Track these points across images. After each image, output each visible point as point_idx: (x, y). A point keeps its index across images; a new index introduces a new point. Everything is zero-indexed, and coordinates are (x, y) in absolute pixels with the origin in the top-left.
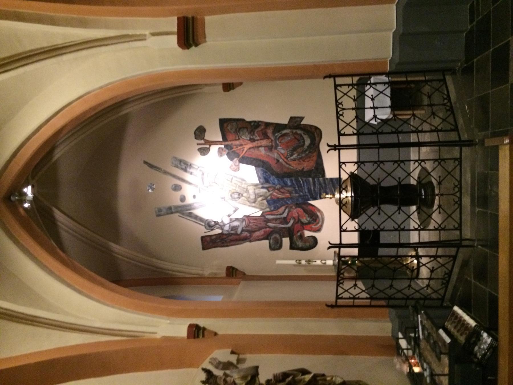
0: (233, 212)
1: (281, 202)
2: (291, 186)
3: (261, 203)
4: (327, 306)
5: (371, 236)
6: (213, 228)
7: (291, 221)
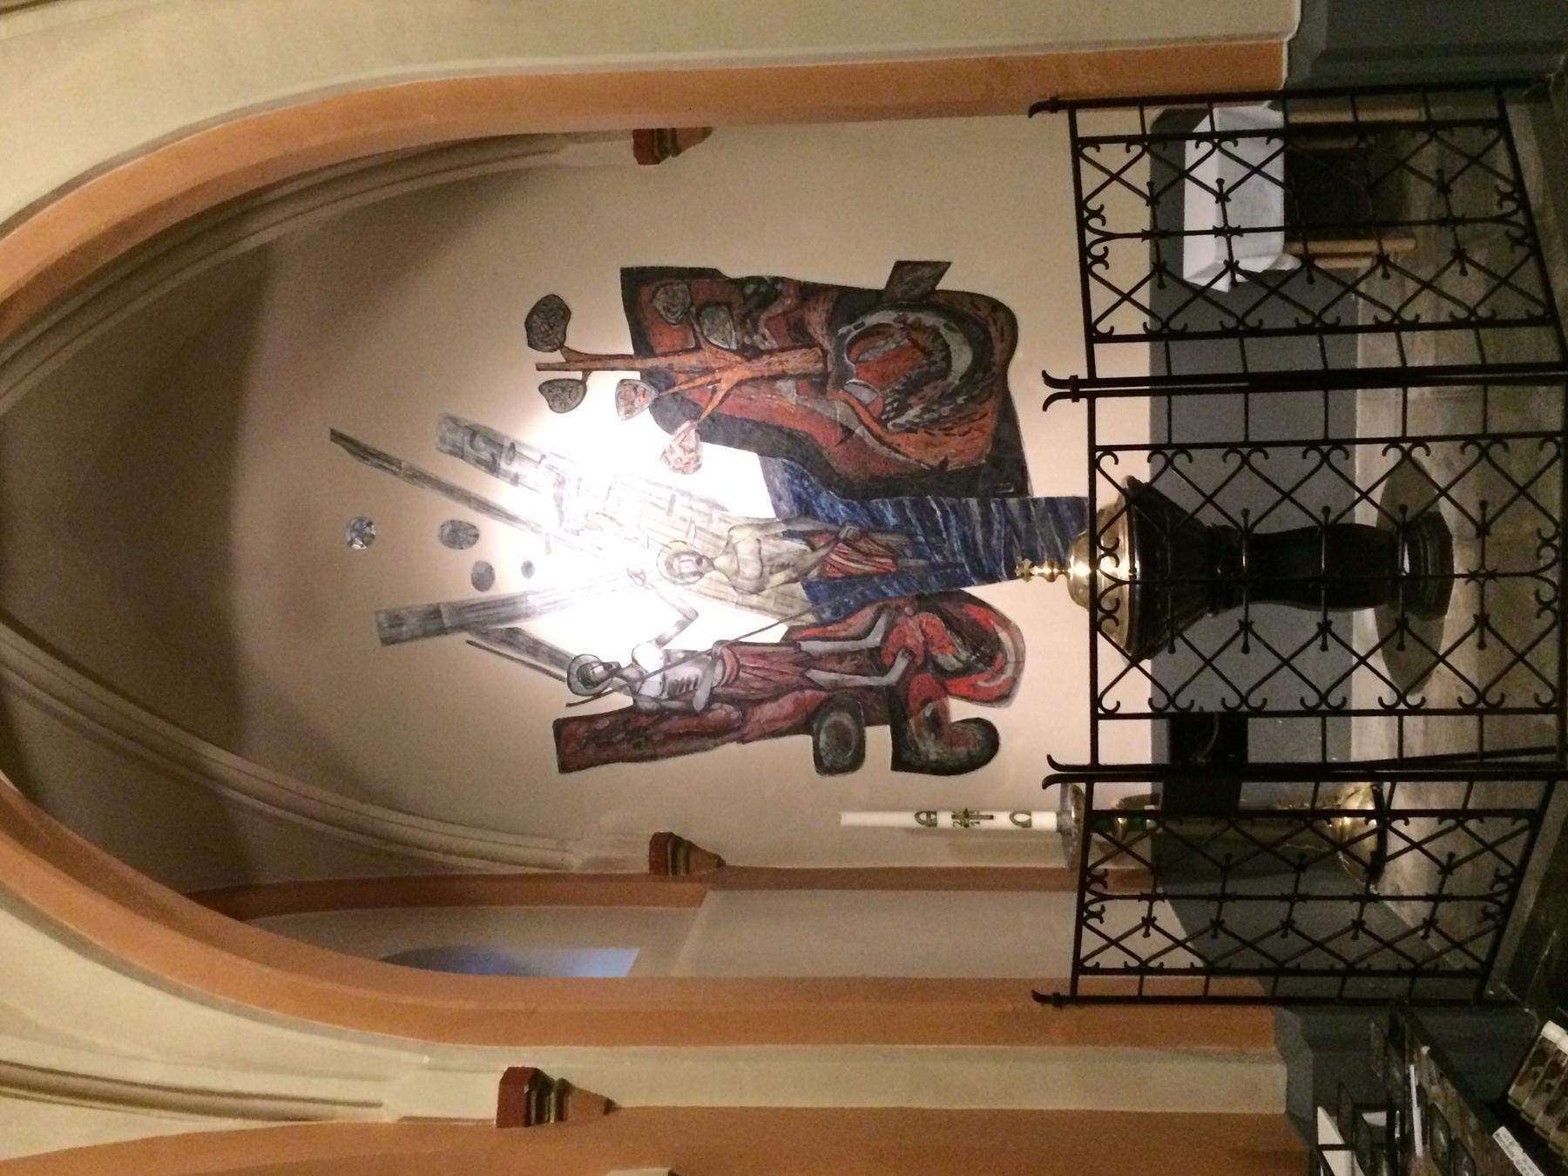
0: (675, 629)
1: (861, 588)
2: (896, 530)
3: (784, 594)
4: (1040, 998)
5: (1216, 733)
6: (599, 688)
7: (896, 663)
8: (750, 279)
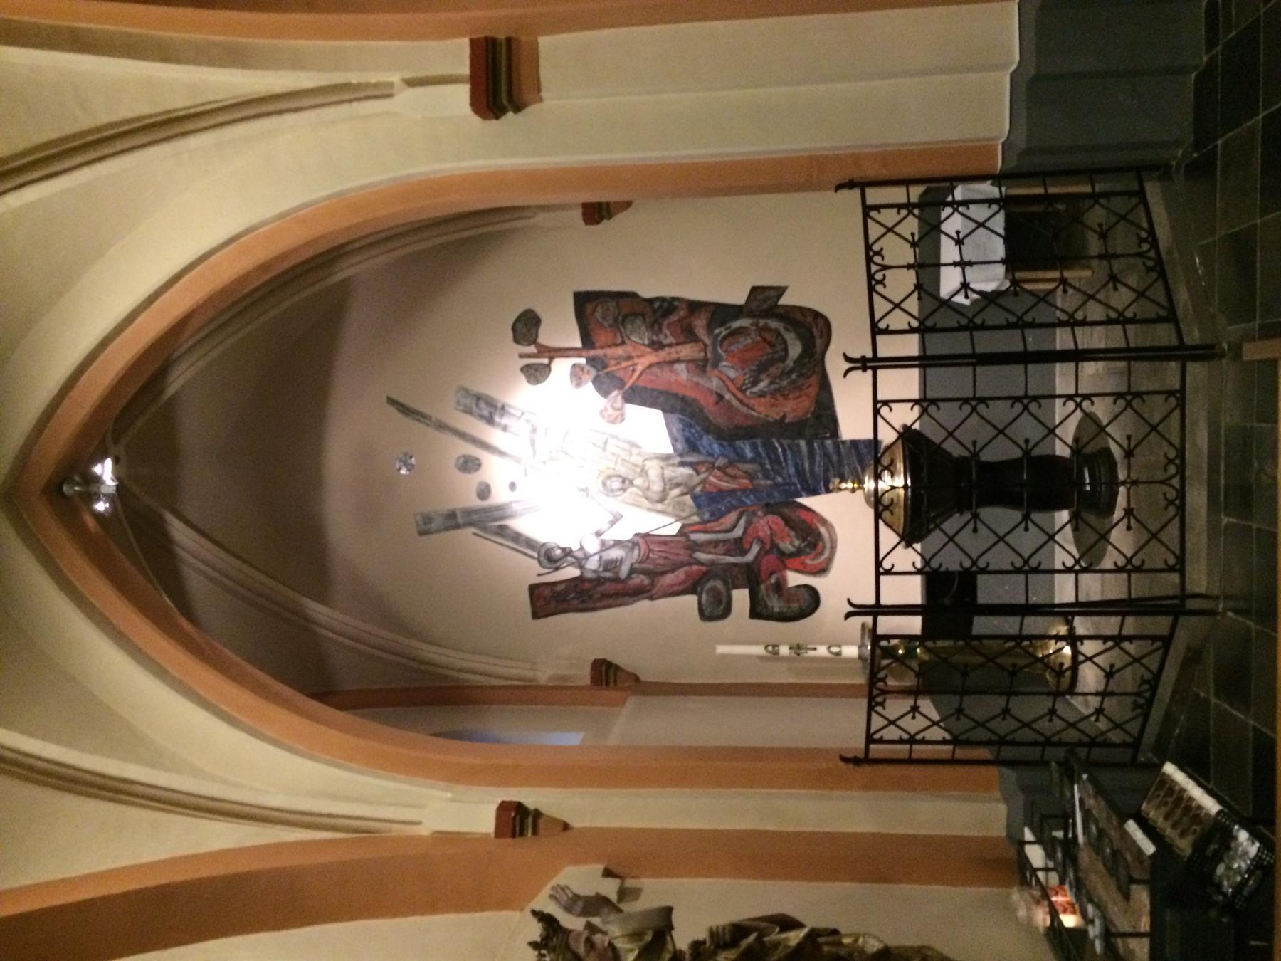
0: (608, 526)
1: (729, 499)
2: (752, 461)
3: (679, 503)
6: (558, 564)
8: (657, 299)
